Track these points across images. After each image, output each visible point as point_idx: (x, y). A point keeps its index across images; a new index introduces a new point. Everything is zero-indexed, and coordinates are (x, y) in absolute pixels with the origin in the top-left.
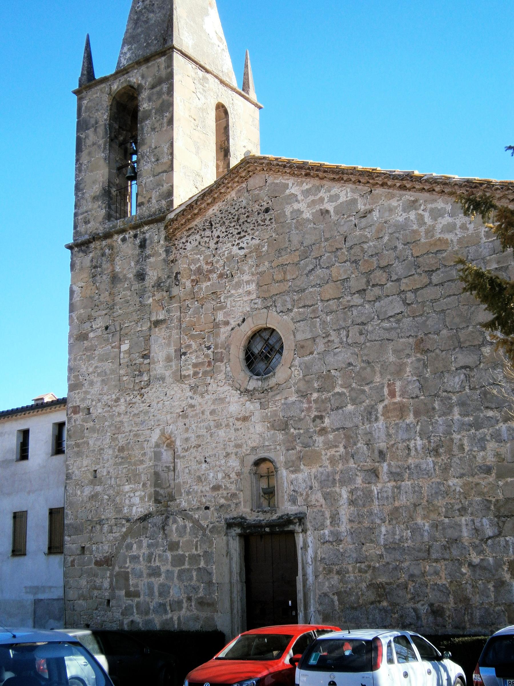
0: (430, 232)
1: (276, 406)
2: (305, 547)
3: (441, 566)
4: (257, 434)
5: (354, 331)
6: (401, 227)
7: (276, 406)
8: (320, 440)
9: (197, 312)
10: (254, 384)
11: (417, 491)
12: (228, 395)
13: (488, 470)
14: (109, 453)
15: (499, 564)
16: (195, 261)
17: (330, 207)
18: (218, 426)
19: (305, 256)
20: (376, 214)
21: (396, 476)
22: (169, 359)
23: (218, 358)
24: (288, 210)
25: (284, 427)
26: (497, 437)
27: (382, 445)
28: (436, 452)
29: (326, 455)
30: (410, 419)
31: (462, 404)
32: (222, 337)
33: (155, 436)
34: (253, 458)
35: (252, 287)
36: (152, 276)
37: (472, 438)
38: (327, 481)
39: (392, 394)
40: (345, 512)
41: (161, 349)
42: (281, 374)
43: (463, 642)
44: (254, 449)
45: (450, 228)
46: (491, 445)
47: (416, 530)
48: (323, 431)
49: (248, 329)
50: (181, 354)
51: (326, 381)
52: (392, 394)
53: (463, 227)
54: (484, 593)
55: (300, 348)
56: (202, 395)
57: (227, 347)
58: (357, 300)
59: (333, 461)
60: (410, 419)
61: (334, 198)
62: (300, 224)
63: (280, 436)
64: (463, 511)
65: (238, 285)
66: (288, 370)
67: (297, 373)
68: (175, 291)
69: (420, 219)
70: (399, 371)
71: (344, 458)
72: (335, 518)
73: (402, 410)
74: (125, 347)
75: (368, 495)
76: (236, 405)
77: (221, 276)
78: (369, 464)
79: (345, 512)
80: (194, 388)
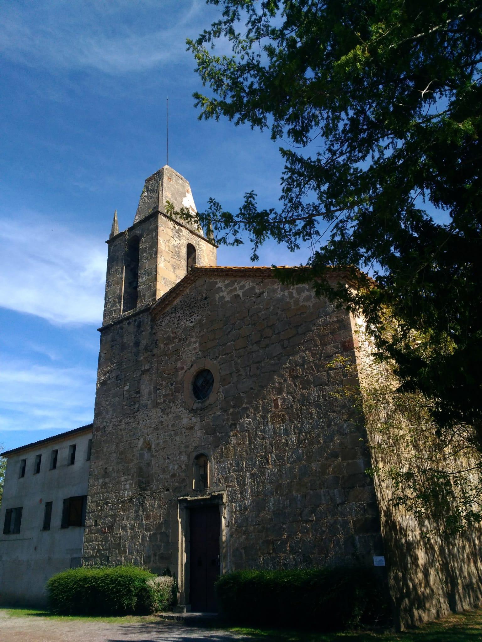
17: (240, 293)
18: (176, 434)
20: (266, 294)
22: (150, 393)
23: (177, 390)
33: (140, 443)
34: (195, 454)
36: (143, 342)
44: (196, 448)
49: (194, 371)
50: (157, 389)
56: (167, 414)
58: (255, 347)
63: (211, 439)
65: (189, 345)
66: (217, 395)
67: (221, 396)
69: (291, 294)
72: (243, 498)
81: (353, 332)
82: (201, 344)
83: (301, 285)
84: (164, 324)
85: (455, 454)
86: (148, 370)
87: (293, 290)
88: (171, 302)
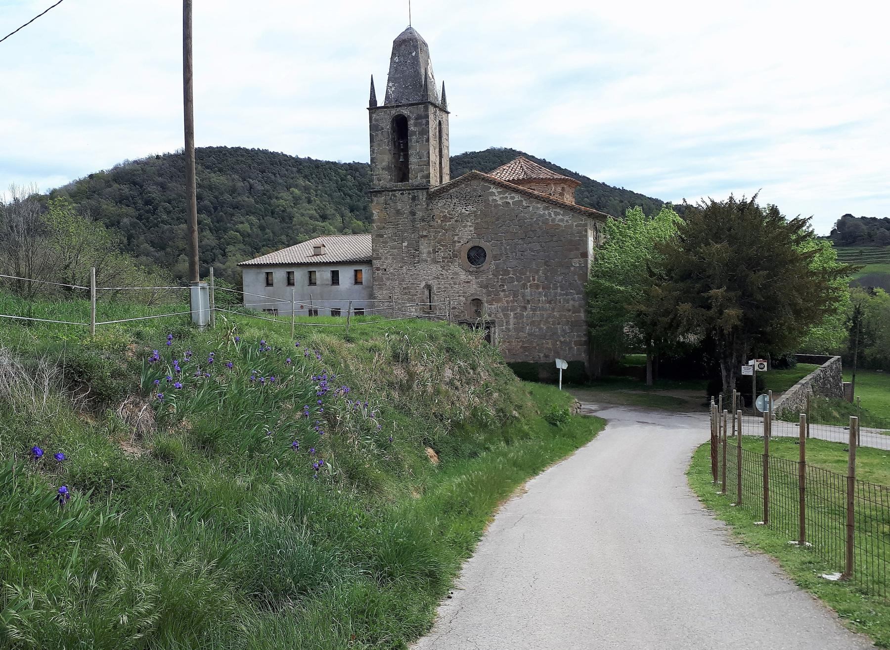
0: (553, 220)
1: (483, 278)
2: (495, 333)
3: (550, 341)
4: (474, 288)
5: (519, 254)
6: (541, 216)
7: (483, 278)
8: (502, 294)
9: (444, 234)
10: (473, 268)
11: (542, 315)
12: (459, 272)
13: (569, 310)
14: (397, 290)
15: (570, 341)
16: (441, 212)
17: (511, 201)
18: (455, 284)
19: (498, 219)
20: (531, 208)
21: (534, 310)
22: (429, 253)
23: (455, 256)
24: (491, 198)
25: (486, 287)
26: (573, 300)
27: (529, 298)
28: (550, 302)
29: (505, 300)
30: (541, 290)
31: (561, 287)
32: (457, 248)
33: (423, 284)
34: (472, 298)
35: (472, 229)
36: (419, 214)
37: (564, 299)
38: (504, 309)
39: (534, 280)
40: (512, 321)
41: (425, 248)
42: (485, 266)
43: (191, 164)
44: (472, 295)
45: (562, 220)
46: (571, 302)
47: (540, 329)
48: (504, 291)
49: (470, 245)
50: (435, 251)
51: (506, 272)
52: (534, 280)
53: (567, 221)
54: (565, 350)
55: (495, 258)
56: (447, 270)
57: (460, 252)
58: (520, 242)
59: (507, 302)
60: (541, 290)
61: (512, 198)
62: (496, 206)
63: (484, 291)
64: (559, 324)
65: (465, 227)
66: (490, 265)
67: (493, 267)
68: (432, 223)
69: (550, 214)
70: (537, 272)
71: (513, 301)
72: (508, 323)
73: (537, 286)
74: (405, 244)
75: (522, 316)
76: (463, 276)
77: (456, 221)
78: (523, 304)
79: (512, 321)
80: (443, 267)
81: (318, 241)
82: (475, 229)
83: (558, 210)
84: (440, 205)
85: (798, 412)
86: (426, 236)
87: (552, 211)
88: (448, 190)
